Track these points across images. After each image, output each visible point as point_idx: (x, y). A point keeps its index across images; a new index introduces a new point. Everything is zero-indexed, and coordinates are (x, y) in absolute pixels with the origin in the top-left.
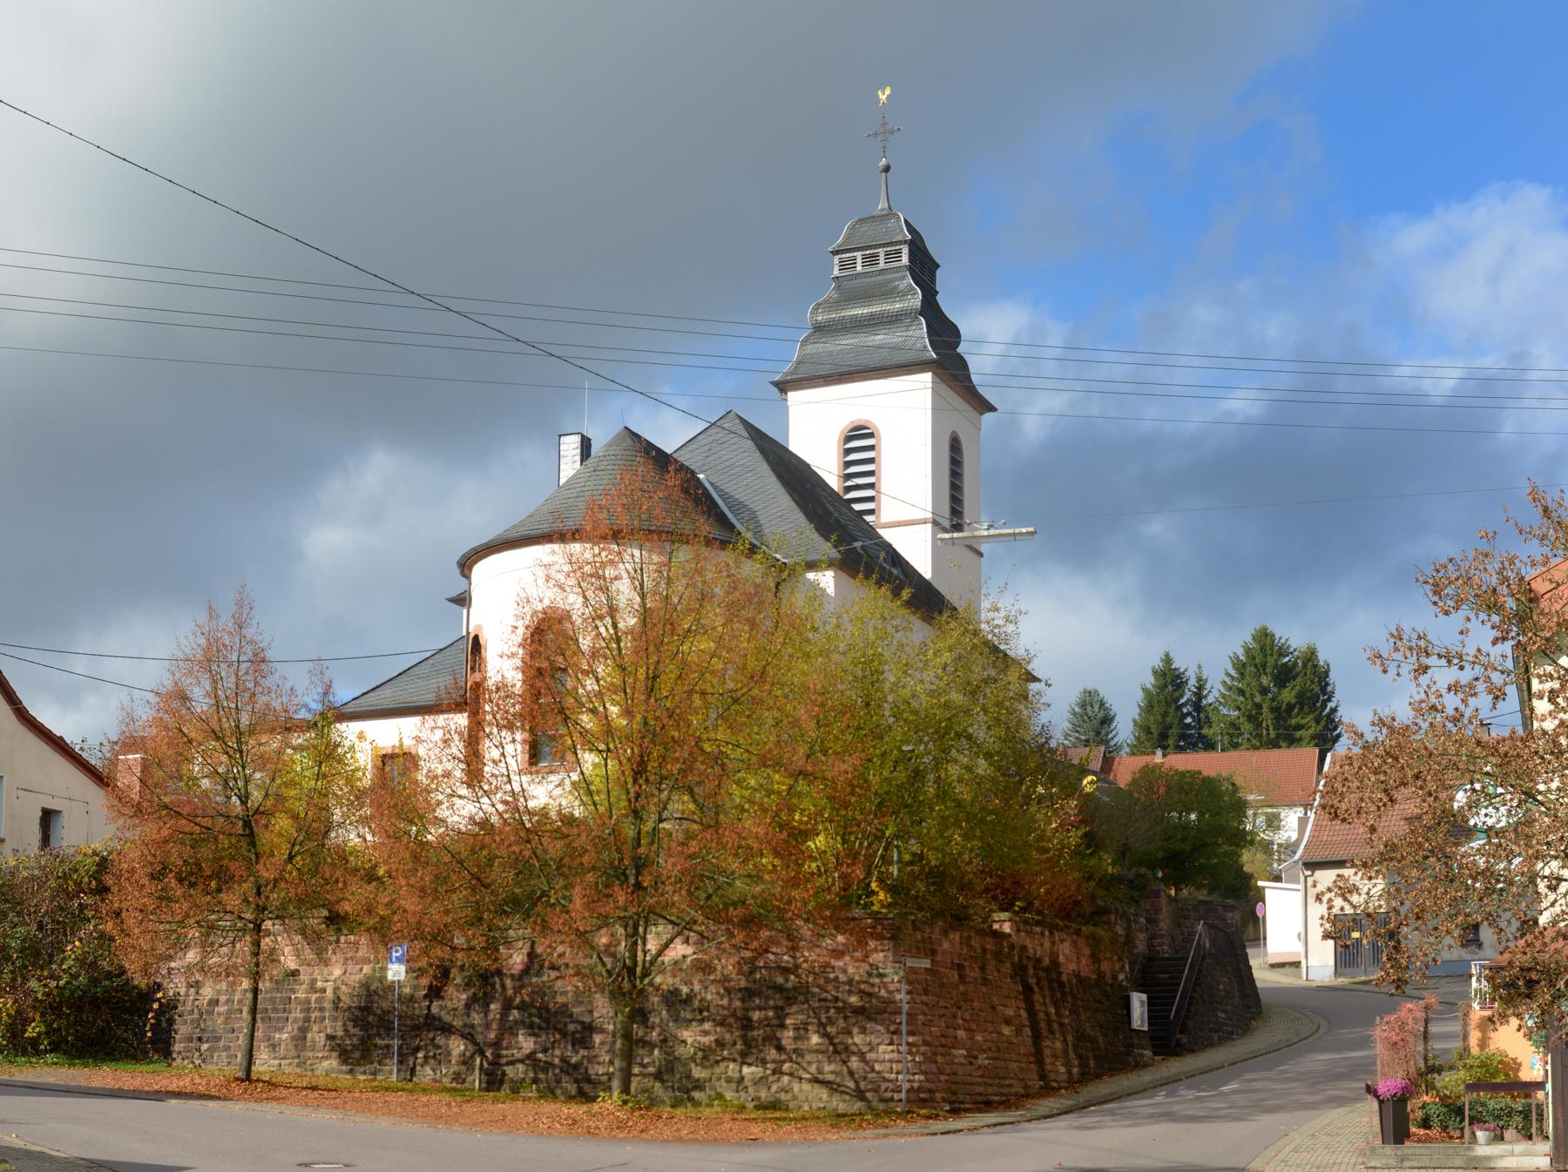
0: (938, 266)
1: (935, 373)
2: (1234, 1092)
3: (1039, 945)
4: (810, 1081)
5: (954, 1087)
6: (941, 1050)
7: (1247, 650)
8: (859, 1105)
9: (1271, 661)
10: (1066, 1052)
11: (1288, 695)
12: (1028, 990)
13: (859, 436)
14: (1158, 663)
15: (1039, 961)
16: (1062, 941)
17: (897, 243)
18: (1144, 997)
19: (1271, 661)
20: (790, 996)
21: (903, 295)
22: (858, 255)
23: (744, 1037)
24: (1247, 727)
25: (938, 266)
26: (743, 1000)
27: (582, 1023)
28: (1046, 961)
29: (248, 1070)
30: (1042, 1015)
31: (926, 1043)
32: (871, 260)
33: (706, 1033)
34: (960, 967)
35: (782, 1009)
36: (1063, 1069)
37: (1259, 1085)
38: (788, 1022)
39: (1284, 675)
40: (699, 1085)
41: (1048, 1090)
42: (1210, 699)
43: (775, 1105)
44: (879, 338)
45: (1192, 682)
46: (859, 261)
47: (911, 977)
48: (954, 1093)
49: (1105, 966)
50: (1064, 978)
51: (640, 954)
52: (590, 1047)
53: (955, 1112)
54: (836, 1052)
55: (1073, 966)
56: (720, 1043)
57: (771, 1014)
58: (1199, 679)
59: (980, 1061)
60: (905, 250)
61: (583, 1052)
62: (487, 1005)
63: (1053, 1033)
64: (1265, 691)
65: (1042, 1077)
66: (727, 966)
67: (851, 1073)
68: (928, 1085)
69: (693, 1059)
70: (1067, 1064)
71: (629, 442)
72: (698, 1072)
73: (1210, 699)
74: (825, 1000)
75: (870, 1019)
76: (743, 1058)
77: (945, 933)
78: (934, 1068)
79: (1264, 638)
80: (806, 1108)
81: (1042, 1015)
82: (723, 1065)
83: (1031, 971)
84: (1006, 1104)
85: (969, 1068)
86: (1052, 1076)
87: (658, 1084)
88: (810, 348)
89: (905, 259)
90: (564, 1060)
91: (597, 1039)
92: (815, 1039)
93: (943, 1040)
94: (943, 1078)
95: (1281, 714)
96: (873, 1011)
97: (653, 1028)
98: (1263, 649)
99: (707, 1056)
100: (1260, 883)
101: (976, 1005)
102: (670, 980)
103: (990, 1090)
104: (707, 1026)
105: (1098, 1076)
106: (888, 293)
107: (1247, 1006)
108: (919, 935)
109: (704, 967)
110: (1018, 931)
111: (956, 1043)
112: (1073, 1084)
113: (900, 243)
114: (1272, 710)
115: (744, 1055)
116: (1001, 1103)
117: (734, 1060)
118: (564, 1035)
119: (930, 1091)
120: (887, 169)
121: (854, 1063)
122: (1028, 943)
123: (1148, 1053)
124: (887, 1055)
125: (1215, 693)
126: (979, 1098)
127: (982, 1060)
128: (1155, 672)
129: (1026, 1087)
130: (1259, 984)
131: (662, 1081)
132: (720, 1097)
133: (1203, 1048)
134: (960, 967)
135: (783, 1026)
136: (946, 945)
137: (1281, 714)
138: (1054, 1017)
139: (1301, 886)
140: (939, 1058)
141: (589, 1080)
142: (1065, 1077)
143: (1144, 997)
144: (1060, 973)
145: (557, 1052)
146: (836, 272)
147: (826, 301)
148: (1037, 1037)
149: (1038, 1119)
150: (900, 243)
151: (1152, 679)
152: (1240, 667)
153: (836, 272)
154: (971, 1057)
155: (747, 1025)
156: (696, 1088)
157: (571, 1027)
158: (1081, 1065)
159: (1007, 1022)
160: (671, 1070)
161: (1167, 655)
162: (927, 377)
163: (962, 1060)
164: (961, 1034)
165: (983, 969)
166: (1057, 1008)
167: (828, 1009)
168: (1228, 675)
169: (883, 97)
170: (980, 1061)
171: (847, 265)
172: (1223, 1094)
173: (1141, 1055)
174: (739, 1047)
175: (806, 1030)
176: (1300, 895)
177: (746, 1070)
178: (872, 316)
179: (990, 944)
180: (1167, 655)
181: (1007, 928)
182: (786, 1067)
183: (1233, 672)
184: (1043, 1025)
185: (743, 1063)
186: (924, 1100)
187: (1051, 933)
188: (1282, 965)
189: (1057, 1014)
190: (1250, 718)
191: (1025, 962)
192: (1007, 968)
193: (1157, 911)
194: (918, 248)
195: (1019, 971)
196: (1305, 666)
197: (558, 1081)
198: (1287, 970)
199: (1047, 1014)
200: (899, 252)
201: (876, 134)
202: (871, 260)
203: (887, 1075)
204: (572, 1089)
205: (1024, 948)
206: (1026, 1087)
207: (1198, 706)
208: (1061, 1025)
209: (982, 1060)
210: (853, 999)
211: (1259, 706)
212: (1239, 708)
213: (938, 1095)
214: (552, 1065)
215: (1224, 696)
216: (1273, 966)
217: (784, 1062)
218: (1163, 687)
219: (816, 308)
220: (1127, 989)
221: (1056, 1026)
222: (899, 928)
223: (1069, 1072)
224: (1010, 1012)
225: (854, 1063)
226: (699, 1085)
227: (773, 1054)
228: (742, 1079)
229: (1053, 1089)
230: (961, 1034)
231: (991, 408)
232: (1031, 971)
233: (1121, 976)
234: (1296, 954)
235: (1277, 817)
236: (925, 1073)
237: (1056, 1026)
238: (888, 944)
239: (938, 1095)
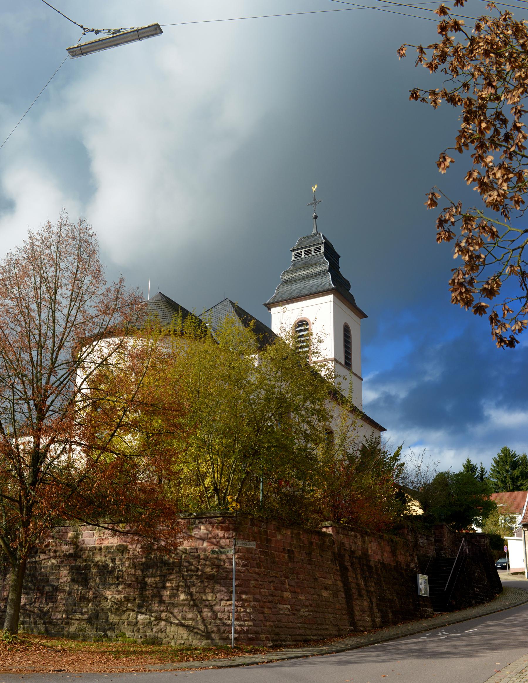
0: (340, 257)
1: (334, 295)
2: (476, 634)
3: (354, 543)
4: (177, 625)
5: (277, 630)
6: (269, 604)
7: (499, 456)
8: (205, 643)
9: (509, 460)
10: (371, 609)
11: (516, 473)
12: (344, 570)
14: (465, 462)
15: (353, 552)
16: (370, 542)
17: (319, 244)
18: (426, 577)
19: (509, 460)
20: (170, 567)
21: (321, 264)
22: (303, 251)
23: (141, 595)
24: (501, 485)
25: (340, 257)
26: (142, 571)
27: (53, 586)
28: (359, 553)
30: (354, 585)
31: (255, 600)
32: (308, 252)
33: (119, 592)
34: (290, 552)
35: (165, 576)
36: (368, 619)
37: (490, 629)
38: (168, 585)
39: (514, 465)
40: (112, 627)
41: (355, 631)
42: (487, 476)
43: (155, 641)
44: (311, 282)
45: (479, 469)
46: (303, 253)
47: (246, 556)
48: (277, 634)
49: (401, 559)
50: (372, 564)
52: (55, 602)
53: (275, 647)
54: (195, 605)
55: (378, 557)
56: (127, 599)
57: (158, 579)
58: (482, 468)
59: (302, 613)
60: (323, 247)
61: (51, 605)
62: (5, 575)
63: (361, 596)
64: (507, 471)
65: (353, 623)
66: (135, 548)
67: (203, 620)
68: (255, 629)
69: (110, 610)
70: (372, 615)
71: (160, 297)
72: (113, 618)
73: (487, 476)
74: (191, 570)
75: (217, 582)
76: (140, 609)
77: (278, 529)
78: (261, 617)
79: (506, 452)
80: (173, 644)
81: (354, 585)
82: (126, 614)
83: (347, 558)
84: (321, 641)
85: (292, 617)
86: (360, 623)
87: (89, 626)
88: (281, 290)
89: (322, 250)
90: (41, 610)
91: (60, 596)
92: (182, 597)
93: (270, 598)
94: (268, 624)
95: (514, 480)
96: (219, 577)
97: (91, 589)
98: (505, 455)
99: (119, 608)
100: (505, 537)
101: (302, 576)
102: (103, 559)
103: (308, 632)
104: (120, 588)
105: (395, 623)
106: (315, 264)
107: (496, 588)
108: (255, 529)
109: (122, 550)
110: (338, 533)
111: (283, 601)
112: (375, 627)
113: (320, 244)
114: (511, 478)
115: (140, 606)
116: (317, 641)
117: (133, 611)
118: (42, 594)
119: (256, 633)
120: (316, 217)
121: (207, 613)
122: (346, 541)
124: (227, 607)
125: (488, 473)
126: (300, 638)
127: (304, 612)
128: (464, 466)
129: (339, 630)
130: (502, 581)
131: (91, 624)
132: (123, 635)
133: (465, 608)
134: (290, 552)
135: (164, 587)
136: (279, 537)
137: (514, 480)
138: (363, 586)
139: (522, 538)
140: (266, 610)
141: (51, 623)
142: (370, 624)
143: (426, 577)
144: (368, 561)
145: (37, 605)
146: (293, 259)
147: (288, 271)
148: (349, 598)
149: (337, 652)
150: (320, 244)
151: (463, 468)
152: (497, 462)
153: (293, 259)
154: (294, 611)
155: (143, 586)
156: (110, 629)
157: (47, 589)
158: (382, 617)
159: (326, 589)
160: (97, 617)
161: (468, 459)
162: (331, 297)
163: (287, 612)
164: (287, 594)
165: (309, 554)
166: (365, 581)
167: (191, 577)
168: (493, 466)
169: (314, 189)
170: (302, 613)
171: (298, 255)
172: (467, 635)
173: (425, 611)
174: (137, 601)
175: (178, 590)
176: (522, 542)
177: (140, 617)
178: (308, 274)
179: (315, 539)
180: (468, 459)
181: (330, 531)
182: (163, 615)
183: (494, 465)
184: (354, 591)
185: (139, 612)
186: (250, 639)
187: (362, 537)
188: (517, 573)
189: (366, 585)
190: (502, 482)
191: (343, 552)
192: (329, 555)
193: (442, 536)
194: (328, 246)
195: (338, 557)
196: (522, 462)
197: (35, 623)
198: (519, 575)
199: (358, 584)
200: (320, 248)
201: (311, 204)
202: (308, 252)
203: (225, 621)
204: (42, 628)
205: (342, 544)
206: (339, 630)
207: (482, 479)
208: (368, 592)
209: (304, 612)
210: (208, 570)
211: (505, 477)
212: (498, 478)
213: (263, 636)
214: (33, 612)
215: (491, 474)
216: (512, 574)
217: (162, 612)
218: (468, 471)
219: (284, 273)
220: (416, 573)
221: (364, 592)
222: (240, 523)
223: (373, 621)
224: (329, 582)
225: (207, 613)
226: (112, 627)
227: (156, 607)
228: (137, 623)
229: (360, 631)
230: (287, 594)
232: (347, 558)
233: (412, 565)
234: (523, 568)
235: (515, 518)
236: (253, 620)
237: (364, 592)
238: (232, 534)
239: (263, 636)
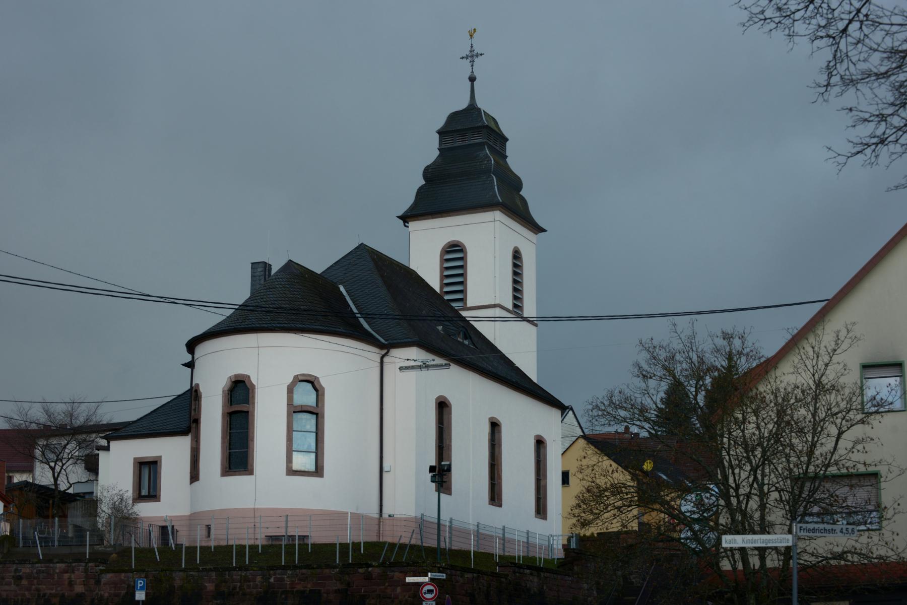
0: (507, 140)
13: (454, 252)
25: (507, 140)
231: (542, 230)
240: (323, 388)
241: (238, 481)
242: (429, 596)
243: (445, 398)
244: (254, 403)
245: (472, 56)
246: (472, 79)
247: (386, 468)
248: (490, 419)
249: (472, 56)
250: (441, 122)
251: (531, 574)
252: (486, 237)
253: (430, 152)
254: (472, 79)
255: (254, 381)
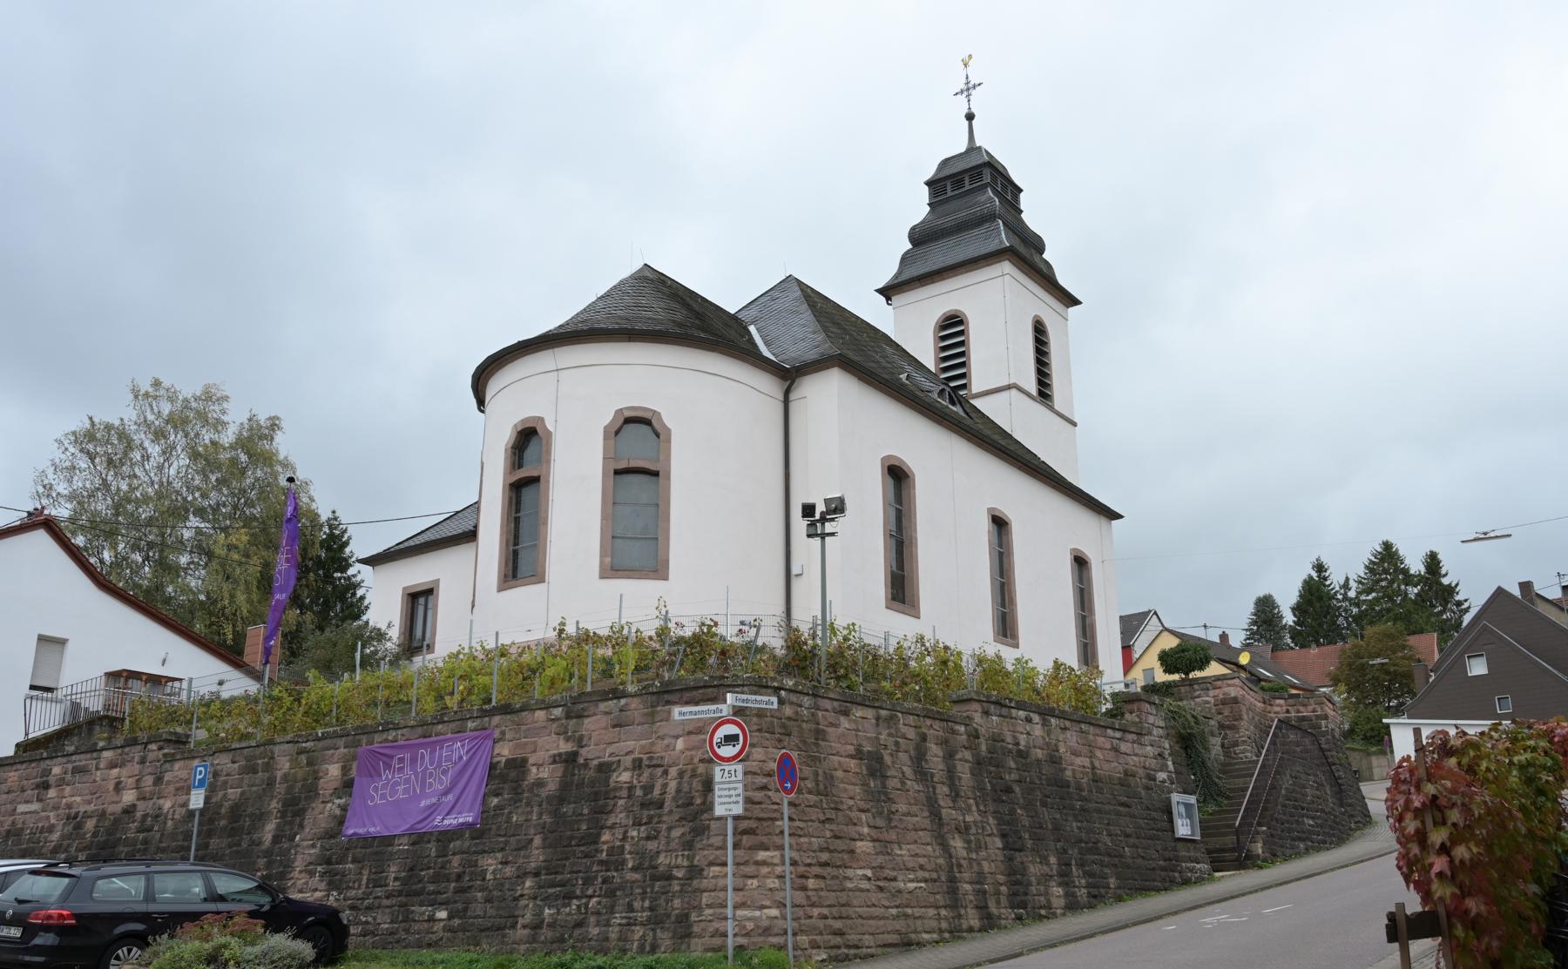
0: (1021, 191)
6: (816, 870)
13: (952, 327)
15: (1022, 755)
25: (1021, 191)
29: (148, 880)
48: (840, 933)
51: (1107, 807)
123: (1204, 867)
140: (811, 883)
231: (1074, 302)
240: (669, 431)
241: (523, 595)
242: (727, 751)
243: (889, 457)
244: (548, 462)
245: (968, 89)
246: (970, 117)
247: (795, 570)
248: (989, 510)
249: (968, 89)
250: (930, 172)
251: (1029, 720)
252: (993, 303)
253: (918, 208)
254: (970, 117)
255: (550, 427)
